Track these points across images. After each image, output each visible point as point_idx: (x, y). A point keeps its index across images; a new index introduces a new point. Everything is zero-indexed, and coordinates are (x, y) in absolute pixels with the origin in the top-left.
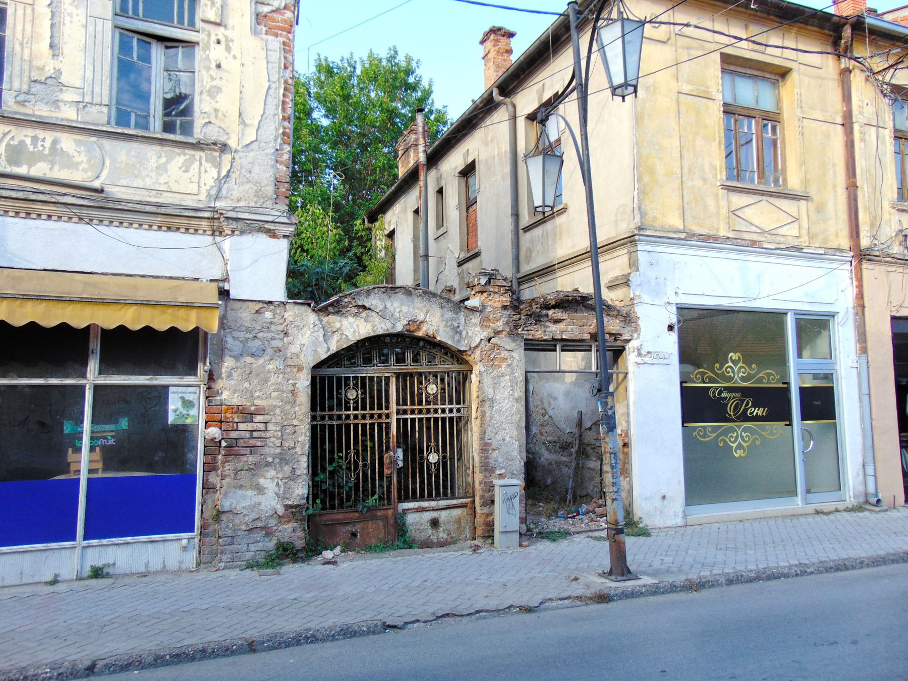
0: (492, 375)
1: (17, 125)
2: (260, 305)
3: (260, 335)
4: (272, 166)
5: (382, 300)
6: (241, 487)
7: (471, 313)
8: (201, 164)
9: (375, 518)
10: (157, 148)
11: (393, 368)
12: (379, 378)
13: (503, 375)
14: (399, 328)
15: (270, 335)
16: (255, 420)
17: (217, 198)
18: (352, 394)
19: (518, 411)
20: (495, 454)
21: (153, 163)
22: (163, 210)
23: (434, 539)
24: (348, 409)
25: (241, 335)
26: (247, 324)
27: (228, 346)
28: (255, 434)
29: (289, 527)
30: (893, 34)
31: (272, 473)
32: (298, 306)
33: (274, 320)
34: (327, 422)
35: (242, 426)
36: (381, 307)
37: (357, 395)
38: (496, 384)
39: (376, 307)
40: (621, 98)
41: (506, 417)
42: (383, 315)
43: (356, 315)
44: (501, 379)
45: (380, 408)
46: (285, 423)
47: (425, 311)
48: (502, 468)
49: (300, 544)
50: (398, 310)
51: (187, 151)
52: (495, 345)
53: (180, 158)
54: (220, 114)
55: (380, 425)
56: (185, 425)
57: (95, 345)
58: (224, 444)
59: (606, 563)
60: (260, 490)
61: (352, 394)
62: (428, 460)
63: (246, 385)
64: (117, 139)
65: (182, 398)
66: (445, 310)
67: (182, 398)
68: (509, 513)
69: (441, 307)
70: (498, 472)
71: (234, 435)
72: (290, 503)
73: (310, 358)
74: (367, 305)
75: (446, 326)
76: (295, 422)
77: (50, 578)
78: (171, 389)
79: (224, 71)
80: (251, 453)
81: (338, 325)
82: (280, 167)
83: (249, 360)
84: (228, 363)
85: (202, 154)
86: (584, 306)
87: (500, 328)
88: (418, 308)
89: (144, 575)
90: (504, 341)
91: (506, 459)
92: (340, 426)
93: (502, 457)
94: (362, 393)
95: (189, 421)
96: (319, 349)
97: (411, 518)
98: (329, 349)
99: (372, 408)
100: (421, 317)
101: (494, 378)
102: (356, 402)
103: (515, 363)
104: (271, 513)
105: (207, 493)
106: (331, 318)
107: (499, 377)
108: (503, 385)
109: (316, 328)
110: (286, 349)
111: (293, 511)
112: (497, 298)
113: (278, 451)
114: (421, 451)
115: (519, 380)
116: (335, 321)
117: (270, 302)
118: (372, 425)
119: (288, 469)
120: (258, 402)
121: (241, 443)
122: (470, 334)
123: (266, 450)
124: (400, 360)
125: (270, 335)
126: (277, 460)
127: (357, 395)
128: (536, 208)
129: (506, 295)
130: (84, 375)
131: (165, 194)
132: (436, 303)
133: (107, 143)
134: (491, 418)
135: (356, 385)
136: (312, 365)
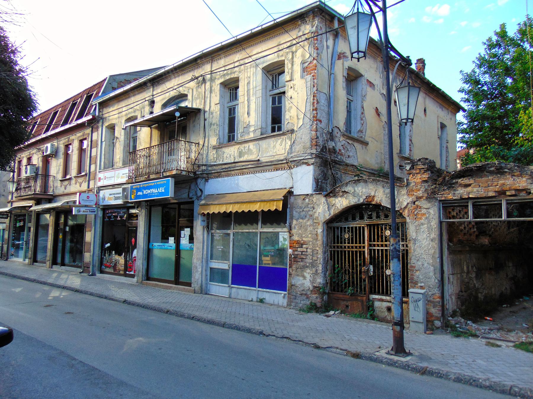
0: (415, 224)
1: (241, 144)
2: (304, 196)
3: (305, 209)
4: (309, 133)
5: (353, 187)
6: (298, 275)
7: (401, 188)
8: (286, 141)
9: (357, 300)
10: (273, 139)
11: (366, 221)
12: (360, 227)
13: (422, 224)
14: (361, 201)
15: (308, 209)
16: (303, 247)
17: (291, 153)
18: (347, 236)
19: (434, 247)
20: (418, 273)
22: (273, 164)
23: (389, 318)
24: (345, 243)
25: (298, 210)
26: (300, 205)
28: (303, 253)
29: (314, 296)
30: (294, 17)
31: (308, 271)
32: (318, 195)
33: (309, 202)
34: (336, 249)
35: (299, 249)
36: (353, 191)
37: (349, 236)
38: (418, 230)
39: (351, 191)
40: (357, 59)
41: (425, 251)
42: (354, 195)
43: (341, 196)
44: (422, 227)
45: (360, 243)
46: (314, 249)
47: (374, 190)
48: (421, 282)
49: (319, 305)
50: (361, 191)
51: (282, 137)
52: (417, 206)
53: (279, 140)
54: (292, 118)
55: (360, 252)
56: (284, 248)
57: (260, 218)
58: (293, 256)
59: (390, 343)
60: (305, 278)
61: (347, 236)
62: (386, 273)
63: (300, 231)
64: (263, 140)
65: (283, 237)
66: (385, 188)
67: (283, 237)
68: (415, 310)
69: (383, 187)
70: (419, 285)
71: (296, 253)
72: (315, 285)
73: (322, 219)
74: (346, 191)
75: (386, 197)
76: (317, 249)
77: (250, 299)
78: (280, 233)
79: (294, 99)
80: (302, 261)
81: (334, 202)
82: (312, 132)
83: (301, 220)
84: (294, 222)
85: (286, 136)
86: (487, 172)
87: (421, 195)
88: (371, 189)
89: (272, 305)
90: (424, 204)
91: (425, 277)
92: (341, 251)
93: (422, 276)
94: (352, 235)
95: (285, 246)
96: (326, 214)
97: (377, 304)
98: (330, 214)
99: (338, 243)
100: (372, 194)
101: (416, 226)
102: (349, 240)
103: (431, 217)
104: (308, 288)
106: (332, 199)
107: (420, 226)
108: (422, 230)
109: (325, 205)
110: (314, 215)
111: (316, 289)
112: (419, 176)
113: (311, 261)
114: (382, 268)
115: (433, 227)
116: (332, 200)
117: (308, 195)
118: (356, 252)
119: (314, 269)
120: (304, 239)
121: (298, 256)
122: (401, 200)
123: (307, 260)
124: (370, 217)
125: (308, 209)
126: (310, 265)
127: (349, 236)
128: (402, 120)
129: (425, 173)
130: (257, 229)
131: (276, 156)
132: (380, 185)
133: (260, 142)
134: (414, 250)
135: (349, 231)
136: (323, 221)
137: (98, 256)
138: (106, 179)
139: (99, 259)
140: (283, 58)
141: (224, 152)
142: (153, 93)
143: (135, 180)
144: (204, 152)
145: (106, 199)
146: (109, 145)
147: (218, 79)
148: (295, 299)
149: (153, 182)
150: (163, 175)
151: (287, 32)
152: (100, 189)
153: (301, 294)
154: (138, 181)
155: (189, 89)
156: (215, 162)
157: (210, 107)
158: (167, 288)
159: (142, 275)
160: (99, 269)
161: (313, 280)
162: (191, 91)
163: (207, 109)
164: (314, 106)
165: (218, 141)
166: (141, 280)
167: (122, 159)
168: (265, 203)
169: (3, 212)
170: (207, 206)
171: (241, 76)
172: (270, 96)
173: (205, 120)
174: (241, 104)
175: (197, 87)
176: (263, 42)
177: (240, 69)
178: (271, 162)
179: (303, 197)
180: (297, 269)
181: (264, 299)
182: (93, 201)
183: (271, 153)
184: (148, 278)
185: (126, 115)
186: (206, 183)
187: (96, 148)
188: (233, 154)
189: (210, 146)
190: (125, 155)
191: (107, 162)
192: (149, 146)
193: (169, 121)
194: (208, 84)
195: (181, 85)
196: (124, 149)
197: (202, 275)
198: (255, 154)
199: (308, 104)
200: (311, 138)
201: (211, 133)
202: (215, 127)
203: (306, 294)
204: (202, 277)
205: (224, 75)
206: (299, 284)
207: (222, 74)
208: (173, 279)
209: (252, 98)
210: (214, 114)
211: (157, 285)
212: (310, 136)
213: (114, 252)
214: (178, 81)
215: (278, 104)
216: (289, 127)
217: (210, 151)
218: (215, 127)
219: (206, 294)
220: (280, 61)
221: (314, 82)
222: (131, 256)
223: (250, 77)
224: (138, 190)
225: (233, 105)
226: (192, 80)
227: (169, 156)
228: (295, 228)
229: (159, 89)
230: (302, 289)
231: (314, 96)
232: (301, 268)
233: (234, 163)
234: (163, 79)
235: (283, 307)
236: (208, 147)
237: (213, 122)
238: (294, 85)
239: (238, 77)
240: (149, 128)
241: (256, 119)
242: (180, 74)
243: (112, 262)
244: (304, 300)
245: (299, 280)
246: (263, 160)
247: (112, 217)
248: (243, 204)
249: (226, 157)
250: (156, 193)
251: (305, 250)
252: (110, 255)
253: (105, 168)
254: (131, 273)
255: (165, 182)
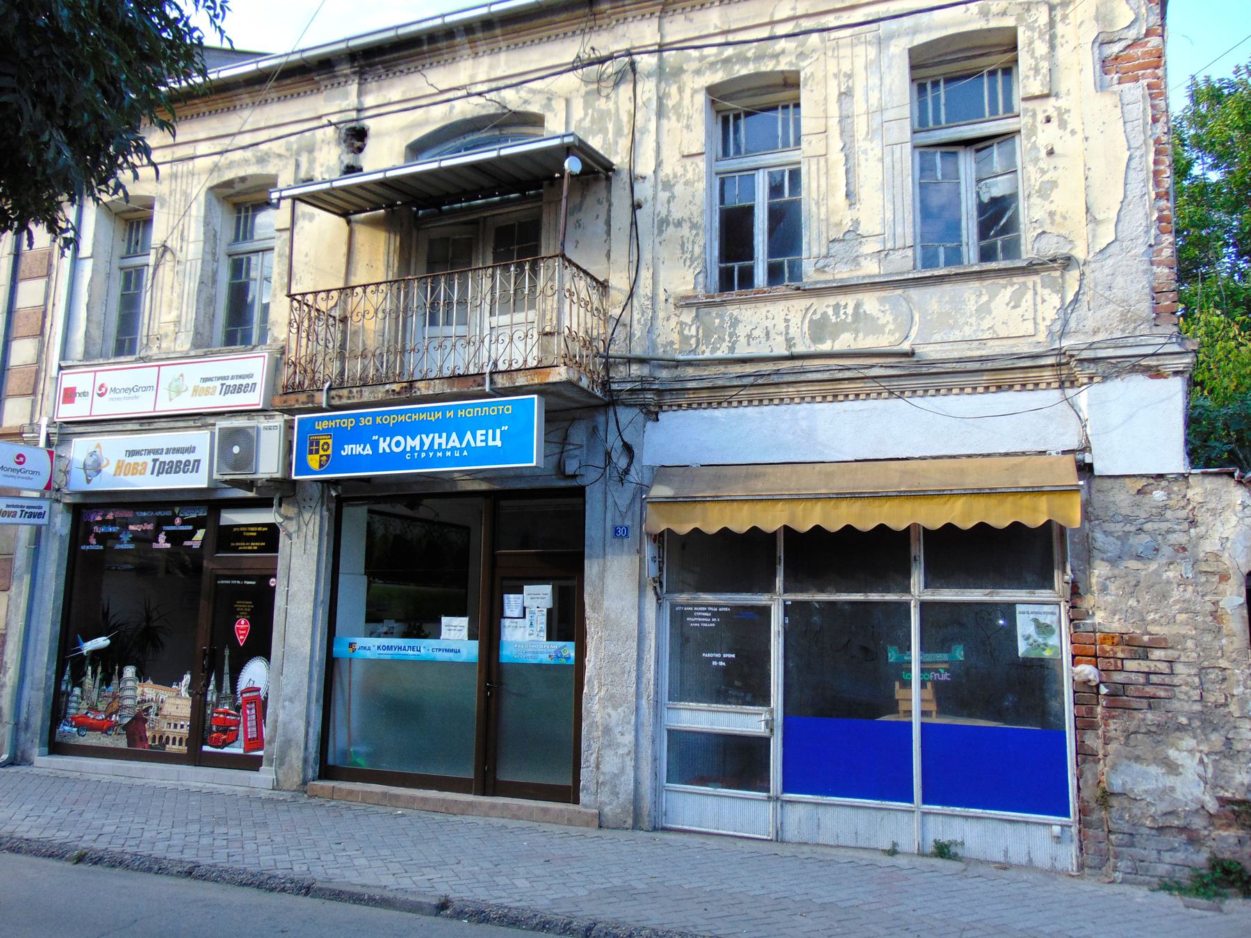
1: (818, 296)
2: (1144, 482)
3: (1148, 526)
4: (1145, 272)
6: (1138, 759)
8: (1036, 294)
10: (975, 285)
15: (1164, 526)
17: (1062, 335)
21: (972, 306)
22: (989, 365)
25: (1118, 528)
27: (1098, 545)
28: (1154, 678)
32: (1210, 478)
33: (1171, 503)
35: (1130, 665)
46: (1206, 664)
53: (1005, 291)
54: (1058, 218)
56: (1042, 660)
57: (918, 550)
60: (1172, 768)
63: (1132, 602)
64: (926, 285)
65: (1036, 621)
72: (1228, 795)
76: (1223, 663)
77: (888, 846)
78: (1019, 608)
80: (1150, 707)
83: (1133, 564)
85: (1037, 278)
95: (1047, 654)
105: (1084, 761)
113: (1197, 707)
119: (1216, 739)
121: (1131, 690)
125: (1164, 526)
126: (1197, 723)
130: (907, 590)
131: (990, 343)
133: (915, 293)
137: (47, 688)
138: (107, 396)
139: (46, 699)
140: (1009, 22)
141: (735, 322)
142: (360, 102)
143: (329, 398)
144: (636, 316)
145: (108, 470)
146: (109, 275)
147: (698, 72)
148: (1132, 845)
149: (437, 409)
150: (492, 382)
151: (417, 71)
152: (65, 432)
153: (1160, 829)
154: (345, 401)
155: (549, 99)
156: (694, 351)
157: (659, 164)
158: (448, 809)
159: (305, 761)
160: (46, 737)
161: (1215, 777)
162: (559, 105)
163: (645, 166)
164: (1157, 184)
165: (701, 278)
166: (296, 779)
167: (191, 326)
168: (809, 504)
169: (416, 483)
170: (689, 507)
171: (807, 70)
172: (717, 174)
173: (636, 206)
174: (813, 161)
175: (587, 93)
176: (558, 41)
177: (803, 45)
178: (981, 359)
179: (1140, 484)
180: (1127, 737)
181: (955, 843)
182: (38, 473)
183: (968, 332)
184: (327, 771)
185: (216, 168)
186: (649, 424)
187: (41, 283)
188: (781, 326)
189: (662, 297)
190: (202, 312)
191: (96, 334)
192: (341, 285)
193: (536, 183)
194: (647, 88)
195: (515, 81)
196: (199, 291)
197: (637, 760)
198: (891, 332)
199: (1137, 178)
200: (1153, 289)
201: (663, 253)
202: (685, 231)
203: (1182, 829)
204: (636, 768)
205: (727, 61)
206: (1146, 791)
207: (712, 59)
208: (470, 774)
209: (861, 143)
210: (679, 189)
211: (397, 797)
212: (1150, 282)
213: (130, 671)
214: (491, 67)
215: (791, 194)
216: (1049, 247)
217: (661, 315)
218: (685, 231)
219: (655, 829)
220: (989, 30)
221: (1153, 107)
222: (226, 679)
223: (849, 76)
224: (342, 437)
225: (745, 166)
226: (578, 65)
227: (491, 314)
228: (1104, 589)
229: (396, 89)
230: (1163, 807)
231: (1157, 152)
232: (1149, 732)
233: (792, 357)
234: (435, 52)
235: (1052, 873)
236: (653, 298)
237: (676, 214)
238: (1061, 112)
239: (798, 73)
240: (341, 221)
241: (889, 215)
242: (502, 44)
243: (122, 707)
244: (1173, 849)
245: (1145, 775)
246: (930, 352)
247: (126, 537)
248: (877, 502)
249: (749, 336)
250: (453, 449)
251: (1163, 667)
252: (107, 681)
253: (87, 355)
254: (227, 750)
255: (509, 410)
